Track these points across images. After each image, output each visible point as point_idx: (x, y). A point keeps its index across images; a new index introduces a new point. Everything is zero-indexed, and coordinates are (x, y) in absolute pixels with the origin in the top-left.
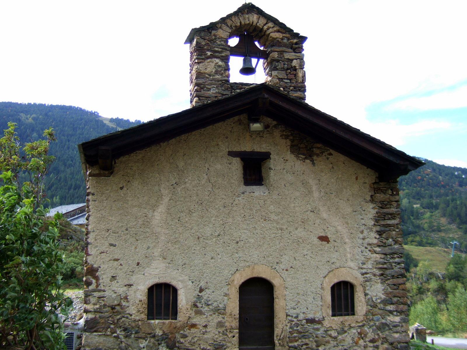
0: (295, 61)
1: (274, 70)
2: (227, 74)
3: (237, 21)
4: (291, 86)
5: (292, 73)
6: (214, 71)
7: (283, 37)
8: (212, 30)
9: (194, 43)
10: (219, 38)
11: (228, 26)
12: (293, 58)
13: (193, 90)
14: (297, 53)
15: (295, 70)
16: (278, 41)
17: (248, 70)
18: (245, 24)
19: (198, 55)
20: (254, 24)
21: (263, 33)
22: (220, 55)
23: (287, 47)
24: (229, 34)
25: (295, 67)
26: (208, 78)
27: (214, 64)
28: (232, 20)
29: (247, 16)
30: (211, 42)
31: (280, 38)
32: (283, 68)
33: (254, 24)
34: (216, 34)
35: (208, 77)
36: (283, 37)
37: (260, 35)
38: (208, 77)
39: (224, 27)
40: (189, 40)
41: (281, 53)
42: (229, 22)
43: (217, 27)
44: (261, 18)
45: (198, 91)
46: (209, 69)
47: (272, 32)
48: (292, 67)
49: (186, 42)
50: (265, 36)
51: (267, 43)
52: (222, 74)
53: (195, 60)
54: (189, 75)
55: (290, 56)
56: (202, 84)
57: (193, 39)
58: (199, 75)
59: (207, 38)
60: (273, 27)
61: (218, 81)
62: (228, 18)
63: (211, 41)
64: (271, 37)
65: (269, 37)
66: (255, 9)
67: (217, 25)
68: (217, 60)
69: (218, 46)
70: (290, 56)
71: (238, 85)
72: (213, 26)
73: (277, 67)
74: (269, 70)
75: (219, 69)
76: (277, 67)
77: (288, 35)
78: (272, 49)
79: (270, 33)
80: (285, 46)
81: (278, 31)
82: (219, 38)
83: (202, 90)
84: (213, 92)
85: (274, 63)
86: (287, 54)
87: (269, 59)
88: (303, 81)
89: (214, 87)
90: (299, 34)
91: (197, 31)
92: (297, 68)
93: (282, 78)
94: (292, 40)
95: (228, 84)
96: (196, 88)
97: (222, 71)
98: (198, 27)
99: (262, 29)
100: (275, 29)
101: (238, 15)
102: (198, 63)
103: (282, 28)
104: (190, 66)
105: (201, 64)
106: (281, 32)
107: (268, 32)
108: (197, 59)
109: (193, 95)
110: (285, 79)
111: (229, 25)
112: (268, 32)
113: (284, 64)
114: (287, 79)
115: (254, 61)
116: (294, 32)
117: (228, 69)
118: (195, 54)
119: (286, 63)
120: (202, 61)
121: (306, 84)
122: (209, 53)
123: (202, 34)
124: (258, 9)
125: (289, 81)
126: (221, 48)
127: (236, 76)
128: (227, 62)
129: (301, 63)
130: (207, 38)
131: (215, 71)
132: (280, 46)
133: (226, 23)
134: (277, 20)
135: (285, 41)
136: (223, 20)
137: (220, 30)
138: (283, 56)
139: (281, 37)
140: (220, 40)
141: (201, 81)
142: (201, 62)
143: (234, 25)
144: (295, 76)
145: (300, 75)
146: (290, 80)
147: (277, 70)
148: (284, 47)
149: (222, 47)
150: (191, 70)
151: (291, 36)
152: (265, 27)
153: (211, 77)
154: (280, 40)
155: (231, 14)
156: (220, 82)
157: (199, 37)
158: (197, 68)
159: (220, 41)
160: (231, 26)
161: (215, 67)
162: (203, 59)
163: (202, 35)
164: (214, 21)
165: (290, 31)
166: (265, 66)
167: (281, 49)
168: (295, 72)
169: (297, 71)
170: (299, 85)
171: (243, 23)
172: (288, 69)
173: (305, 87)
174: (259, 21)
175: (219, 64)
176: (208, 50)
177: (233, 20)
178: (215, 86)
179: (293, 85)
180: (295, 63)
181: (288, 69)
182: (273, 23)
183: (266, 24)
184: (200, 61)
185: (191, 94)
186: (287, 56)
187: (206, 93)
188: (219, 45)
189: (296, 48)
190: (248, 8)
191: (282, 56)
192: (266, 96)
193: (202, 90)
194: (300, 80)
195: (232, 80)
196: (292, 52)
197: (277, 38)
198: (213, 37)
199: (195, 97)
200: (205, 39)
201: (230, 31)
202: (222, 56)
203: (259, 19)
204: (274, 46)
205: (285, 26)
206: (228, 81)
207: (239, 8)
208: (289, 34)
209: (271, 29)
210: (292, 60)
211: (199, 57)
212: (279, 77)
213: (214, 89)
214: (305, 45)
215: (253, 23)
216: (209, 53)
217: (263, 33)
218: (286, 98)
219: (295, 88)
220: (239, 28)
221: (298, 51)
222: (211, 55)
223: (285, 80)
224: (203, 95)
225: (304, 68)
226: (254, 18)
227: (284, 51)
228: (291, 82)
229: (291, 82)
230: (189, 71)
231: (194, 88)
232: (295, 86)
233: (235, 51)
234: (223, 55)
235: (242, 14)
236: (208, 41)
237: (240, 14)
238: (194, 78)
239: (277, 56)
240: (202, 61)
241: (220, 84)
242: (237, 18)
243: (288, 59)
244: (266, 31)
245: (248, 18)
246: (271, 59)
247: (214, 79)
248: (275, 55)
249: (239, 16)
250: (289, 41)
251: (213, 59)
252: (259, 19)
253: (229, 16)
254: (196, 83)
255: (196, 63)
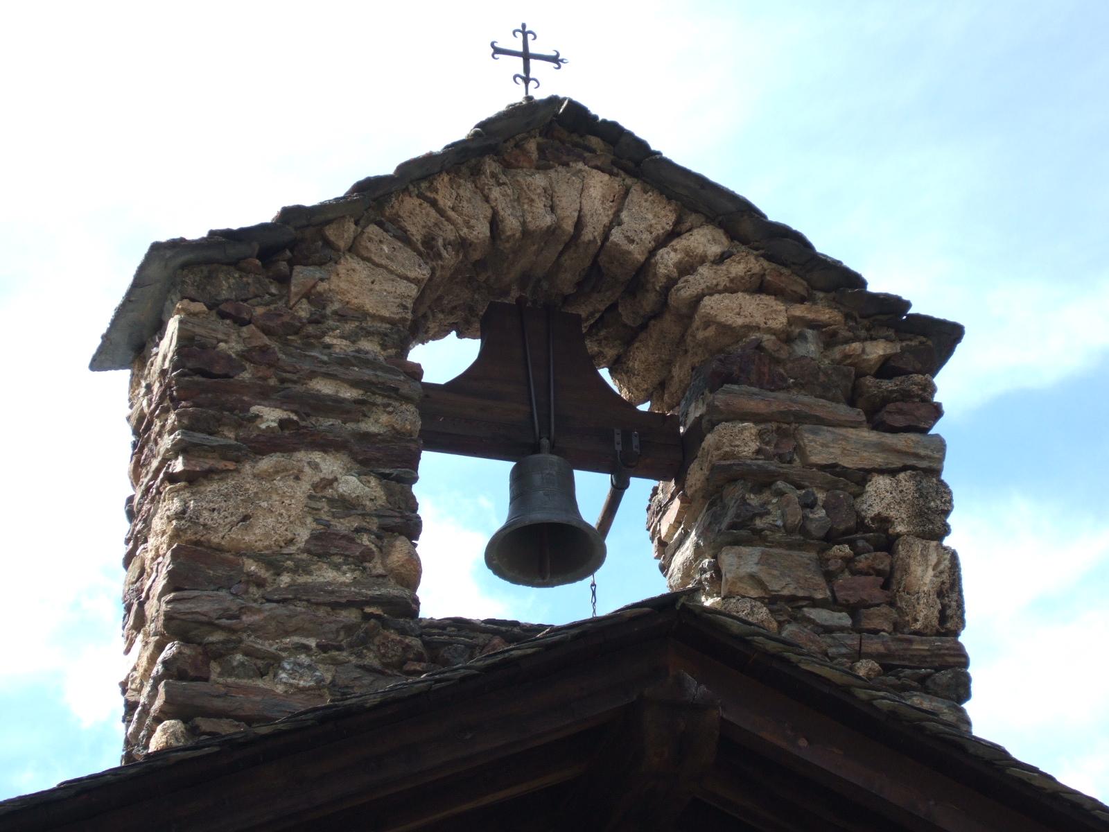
0: (881, 483)
1: (736, 542)
2: (397, 557)
3: (468, 213)
4: (860, 655)
5: (863, 562)
6: (303, 535)
7: (792, 321)
8: (292, 263)
9: (167, 345)
10: (342, 317)
11: (405, 239)
12: (866, 465)
13: (147, 670)
14: (894, 430)
15: (888, 543)
16: (759, 347)
17: (542, 545)
18: (526, 233)
19: (190, 425)
20: (591, 232)
21: (649, 301)
22: (350, 426)
23: (825, 392)
24: (413, 291)
25: (883, 521)
26: (260, 584)
27: (305, 486)
28: (434, 203)
29: (539, 180)
30: (286, 343)
31: (770, 331)
32: (803, 529)
33: (591, 232)
34: (322, 287)
35: (264, 574)
36: (792, 321)
37: (627, 316)
38: (264, 574)
39: (380, 244)
40: (125, 344)
41: (783, 429)
42: (415, 215)
43: (328, 243)
44: (636, 195)
45: (182, 676)
46: (271, 521)
47: (712, 291)
48: (861, 525)
49: (99, 363)
50: (668, 323)
51: (679, 372)
52: (366, 556)
53: (165, 461)
54: (118, 581)
55: (845, 452)
56: (212, 626)
57: (159, 328)
58: (195, 563)
59: (260, 310)
60: (721, 259)
61: (336, 606)
62: (406, 190)
63: (285, 331)
64: (708, 322)
65: (697, 321)
66: (595, 141)
67: (330, 232)
68: (330, 465)
69: (339, 370)
70: (845, 452)
71: (481, 638)
72: (298, 237)
73: (759, 523)
74: (698, 552)
75: (344, 525)
76: (759, 523)
77: (825, 314)
78: (720, 399)
79: (698, 299)
80: (808, 379)
81: (760, 287)
82: (342, 317)
83: (215, 668)
84: (296, 680)
85: (735, 492)
86: (826, 434)
87: (696, 475)
88: (943, 618)
89: (306, 648)
90: (907, 305)
91: (184, 266)
92: (900, 528)
93: (792, 599)
94: (856, 346)
95: (403, 632)
96: (169, 651)
97: (365, 540)
98: (196, 232)
99: (646, 267)
100: (737, 269)
101: (476, 172)
102: (191, 479)
103: (785, 257)
104: (131, 515)
105: (211, 488)
106: (778, 293)
107: (687, 289)
108: (178, 449)
109: (145, 711)
110: (814, 603)
111: (417, 234)
112: (687, 289)
113: (809, 505)
114: (833, 604)
115: (591, 490)
116: (872, 288)
117: (411, 528)
118: (172, 417)
119: (821, 496)
120: (221, 465)
121: (964, 638)
122: (270, 416)
123: (226, 286)
124: (613, 134)
125: (844, 619)
126: (355, 384)
127: (456, 571)
128: (399, 479)
129: (922, 494)
130: (260, 310)
131: (315, 537)
132: (776, 384)
133: (395, 220)
134: (746, 209)
135: (810, 348)
136: (372, 196)
137: (351, 262)
138: (799, 449)
139: (780, 322)
140: (350, 326)
141: (206, 604)
142: (208, 474)
143: (451, 236)
144: (886, 586)
145: (924, 577)
146: (854, 610)
147: (756, 537)
148: (800, 386)
149: (367, 374)
150: (137, 539)
151: (848, 316)
152: (669, 258)
153: (285, 579)
154: (768, 340)
155: (430, 159)
156: (350, 616)
157: (199, 307)
158: (180, 515)
159: (352, 337)
160: (429, 241)
161: (313, 511)
162: (224, 452)
163: (225, 294)
164: (310, 199)
165: (842, 282)
166: (664, 529)
167: (779, 401)
168: (882, 561)
169: (902, 551)
170: (920, 646)
171: (511, 224)
172: (831, 538)
173: (960, 659)
174: (624, 215)
175: (342, 488)
176: (265, 395)
177: (445, 201)
178: (312, 642)
179: (874, 646)
180: (881, 497)
181: (831, 538)
182: (720, 235)
183: (674, 234)
184: (207, 464)
185: (130, 707)
186: (822, 448)
187: (246, 690)
188: (344, 362)
189: (886, 400)
190: (547, 132)
191: (787, 448)
192: (696, 689)
193: (215, 668)
194: (925, 613)
195: (435, 602)
196: (855, 425)
197: (749, 328)
198: (304, 311)
199: (158, 720)
200: (240, 322)
201: (423, 272)
202: (366, 436)
203: (621, 199)
204: (730, 379)
205: (807, 246)
206: (410, 607)
207: (482, 125)
208: (836, 303)
209: (704, 270)
210: (862, 477)
211: (199, 437)
212: (775, 586)
213: (303, 658)
214: (950, 384)
215: (579, 224)
216: (270, 416)
217: (649, 301)
218: (831, 705)
219: (887, 669)
220: (480, 265)
221: (899, 421)
222: (283, 424)
223: (813, 613)
224: (219, 703)
225: (946, 530)
226: (589, 193)
227: (802, 418)
228: (856, 628)
229: (856, 628)
230: (123, 550)
231: (152, 660)
232: (890, 655)
233: (458, 420)
234: (369, 426)
235: (507, 166)
236: (267, 331)
237: (490, 166)
238: (161, 583)
239: (754, 446)
240: (221, 465)
241: (349, 629)
242: (467, 189)
243: (832, 468)
244: (671, 282)
245: (549, 194)
246: (713, 468)
247: (306, 588)
248: (744, 441)
249: (485, 180)
250: (837, 353)
251: (301, 455)
252: (621, 199)
253: (419, 173)
254: (169, 617)
255: (172, 478)
